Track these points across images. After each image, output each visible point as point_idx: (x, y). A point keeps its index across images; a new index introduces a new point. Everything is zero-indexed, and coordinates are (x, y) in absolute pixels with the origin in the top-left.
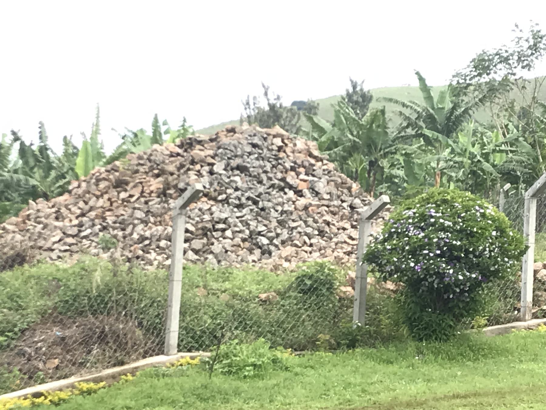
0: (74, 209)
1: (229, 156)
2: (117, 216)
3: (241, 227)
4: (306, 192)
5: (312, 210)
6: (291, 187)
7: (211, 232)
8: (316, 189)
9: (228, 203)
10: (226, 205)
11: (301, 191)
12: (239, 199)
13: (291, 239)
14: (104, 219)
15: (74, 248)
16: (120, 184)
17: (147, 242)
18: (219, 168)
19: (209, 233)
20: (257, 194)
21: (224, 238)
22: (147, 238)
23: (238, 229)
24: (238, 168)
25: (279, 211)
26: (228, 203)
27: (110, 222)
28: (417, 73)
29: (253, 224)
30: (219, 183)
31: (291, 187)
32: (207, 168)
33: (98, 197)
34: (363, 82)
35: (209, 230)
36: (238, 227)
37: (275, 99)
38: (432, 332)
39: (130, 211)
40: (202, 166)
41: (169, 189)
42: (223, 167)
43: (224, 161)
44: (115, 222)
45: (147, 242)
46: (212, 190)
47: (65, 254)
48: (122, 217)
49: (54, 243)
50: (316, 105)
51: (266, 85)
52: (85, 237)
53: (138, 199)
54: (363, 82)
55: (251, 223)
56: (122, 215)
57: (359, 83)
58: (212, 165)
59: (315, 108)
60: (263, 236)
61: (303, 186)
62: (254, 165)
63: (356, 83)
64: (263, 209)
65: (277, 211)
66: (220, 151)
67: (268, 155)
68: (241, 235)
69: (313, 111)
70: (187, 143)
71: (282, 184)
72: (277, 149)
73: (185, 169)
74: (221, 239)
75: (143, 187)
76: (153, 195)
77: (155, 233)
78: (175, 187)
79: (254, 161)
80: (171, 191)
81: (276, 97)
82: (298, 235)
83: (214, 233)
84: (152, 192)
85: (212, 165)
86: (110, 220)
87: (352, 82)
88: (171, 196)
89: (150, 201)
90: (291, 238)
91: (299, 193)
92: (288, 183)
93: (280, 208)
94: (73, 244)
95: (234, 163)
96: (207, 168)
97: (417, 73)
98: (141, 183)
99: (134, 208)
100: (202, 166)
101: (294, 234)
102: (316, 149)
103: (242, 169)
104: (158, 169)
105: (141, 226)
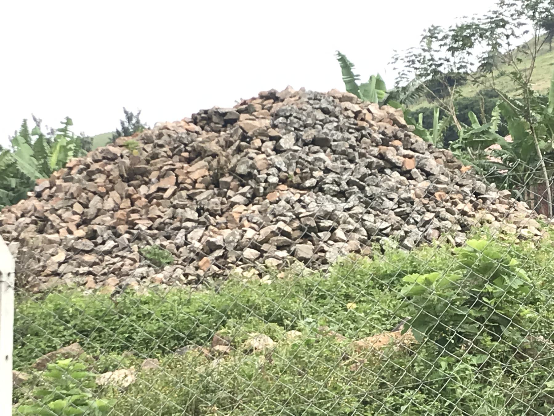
0: (66, 215)
1: (296, 126)
2: (152, 219)
3: (353, 224)
4: (416, 172)
5: (440, 196)
6: (394, 167)
7: (316, 233)
8: (427, 169)
9: (321, 190)
10: (320, 193)
11: (409, 171)
12: (339, 184)
13: (426, 238)
14: (132, 225)
15: (96, 269)
16: (134, 175)
17: (219, 253)
18: (287, 142)
19: (313, 234)
20: (359, 176)
21: (336, 241)
22: (219, 247)
23: (351, 227)
24: (315, 142)
25: (396, 200)
26: (321, 190)
27: (144, 228)
28: (343, 60)
29: (369, 219)
30: (297, 163)
31: (394, 167)
32: (270, 145)
33: (102, 196)
34: (139, 114)
35: (311, 229)
36: (349, 223)
37: (48, 134)
38: (461, 378)
39: (170, 211)
40: (263, 142)
41: (223, 175)
42: (293, 141)
43: (291, 133)
44: (150, 228)
45: (219, 253)
46: (291, 173)
47: (85, 279)
48: (159, 221)
49: (60, 264)
50: (89, 140)
51: (37, 118)
52: (109, 252)
53: (174, 194)
54: (139, 114)
55: (366, 217)
56: (159, 217)
57: (135, 114)
58: (277, 139)
59: (89, 143)
60: (387, 235)
61: (410, 165)
62: (335, 137)
63: (132, 115)
64: (372, 198)
65: (392, 200)
66: (281, 119)
67: (347, 124)
68: (357, 236)
69: (87, 146)
70: (203, 119)
71: (382, 162)
72: (353, 115)
73: (234, 147)
74: (331, 242)
75: (177, 176)
76: (197, 185)
77: (231, 238)
78: (232, 171)
79: (334, 132)
80: (228, 179)
81: (50, 131)
82: (436, 233)
83: (320, 234)
84: (195, 182)
85: (277, 139)
86: (143, 225)
87: (126, 112)
88: (228, 186)
89: (196, 194)
90: (425, 237)
91: (407, 174)
92: (388, 161)
93: (394, 195)
94: (95, 264)
95: (308, 134)
96: (270, 145)
97: (343, 60)
98: (173, 170)
99: (175, 207)
100: (263, 142)
101: (430, 231)
102: (401, 116)
103: (322, 143)
104: (186, 151)
105: (200, 231)
